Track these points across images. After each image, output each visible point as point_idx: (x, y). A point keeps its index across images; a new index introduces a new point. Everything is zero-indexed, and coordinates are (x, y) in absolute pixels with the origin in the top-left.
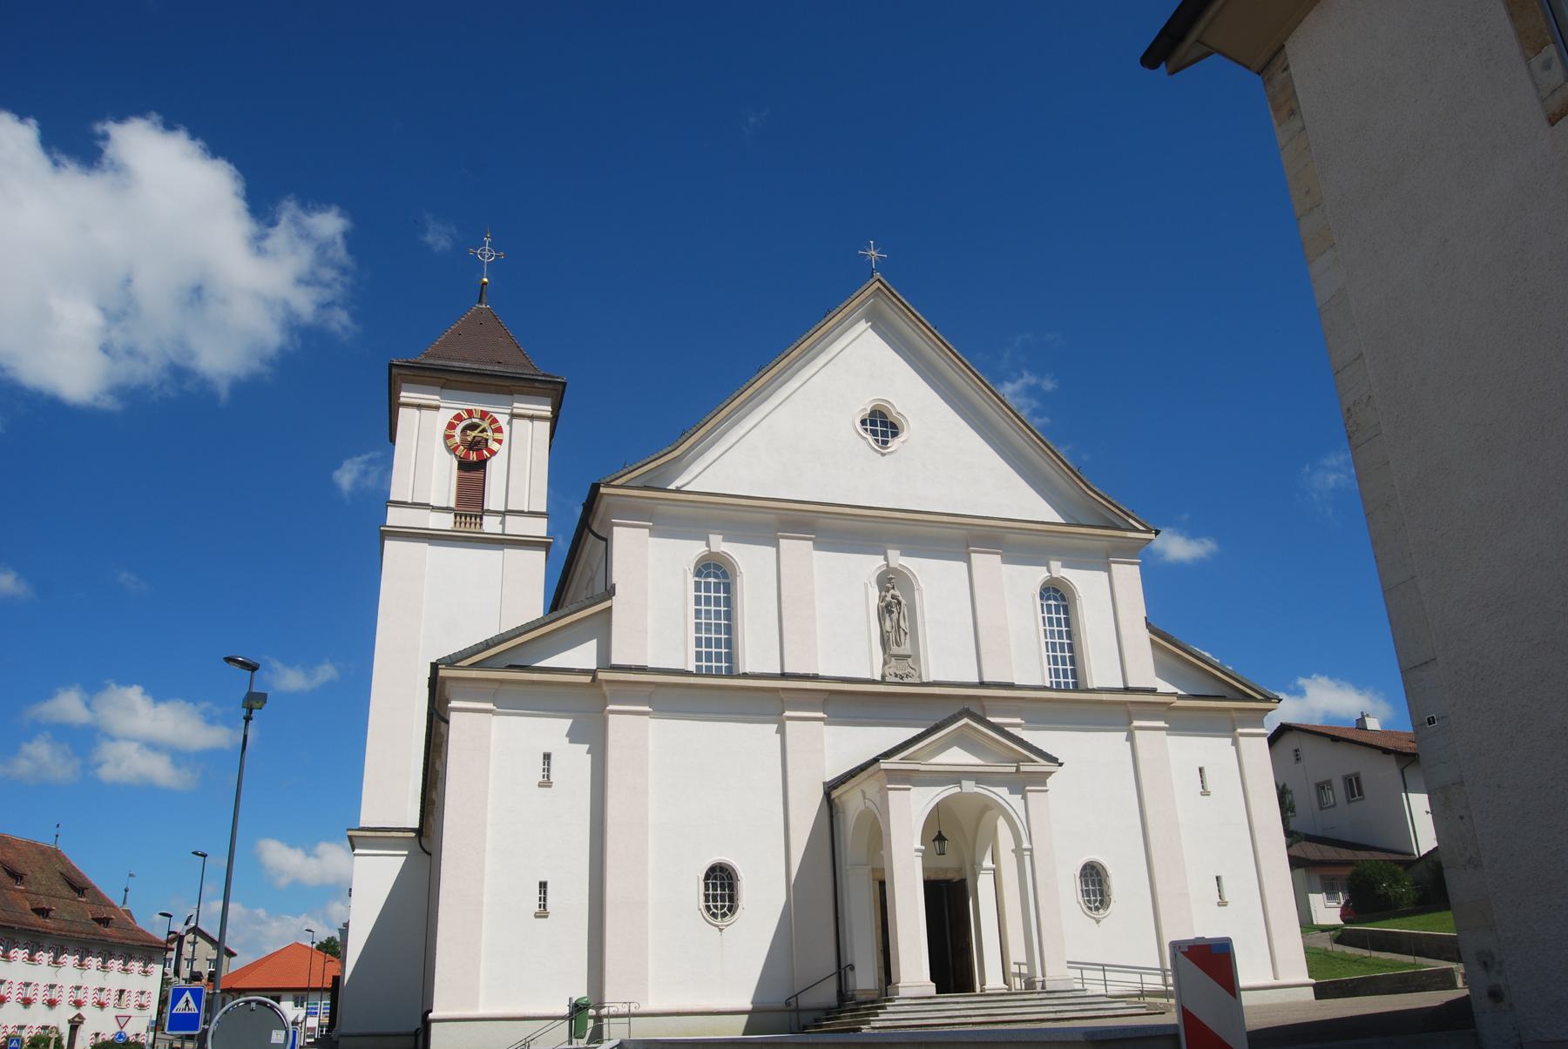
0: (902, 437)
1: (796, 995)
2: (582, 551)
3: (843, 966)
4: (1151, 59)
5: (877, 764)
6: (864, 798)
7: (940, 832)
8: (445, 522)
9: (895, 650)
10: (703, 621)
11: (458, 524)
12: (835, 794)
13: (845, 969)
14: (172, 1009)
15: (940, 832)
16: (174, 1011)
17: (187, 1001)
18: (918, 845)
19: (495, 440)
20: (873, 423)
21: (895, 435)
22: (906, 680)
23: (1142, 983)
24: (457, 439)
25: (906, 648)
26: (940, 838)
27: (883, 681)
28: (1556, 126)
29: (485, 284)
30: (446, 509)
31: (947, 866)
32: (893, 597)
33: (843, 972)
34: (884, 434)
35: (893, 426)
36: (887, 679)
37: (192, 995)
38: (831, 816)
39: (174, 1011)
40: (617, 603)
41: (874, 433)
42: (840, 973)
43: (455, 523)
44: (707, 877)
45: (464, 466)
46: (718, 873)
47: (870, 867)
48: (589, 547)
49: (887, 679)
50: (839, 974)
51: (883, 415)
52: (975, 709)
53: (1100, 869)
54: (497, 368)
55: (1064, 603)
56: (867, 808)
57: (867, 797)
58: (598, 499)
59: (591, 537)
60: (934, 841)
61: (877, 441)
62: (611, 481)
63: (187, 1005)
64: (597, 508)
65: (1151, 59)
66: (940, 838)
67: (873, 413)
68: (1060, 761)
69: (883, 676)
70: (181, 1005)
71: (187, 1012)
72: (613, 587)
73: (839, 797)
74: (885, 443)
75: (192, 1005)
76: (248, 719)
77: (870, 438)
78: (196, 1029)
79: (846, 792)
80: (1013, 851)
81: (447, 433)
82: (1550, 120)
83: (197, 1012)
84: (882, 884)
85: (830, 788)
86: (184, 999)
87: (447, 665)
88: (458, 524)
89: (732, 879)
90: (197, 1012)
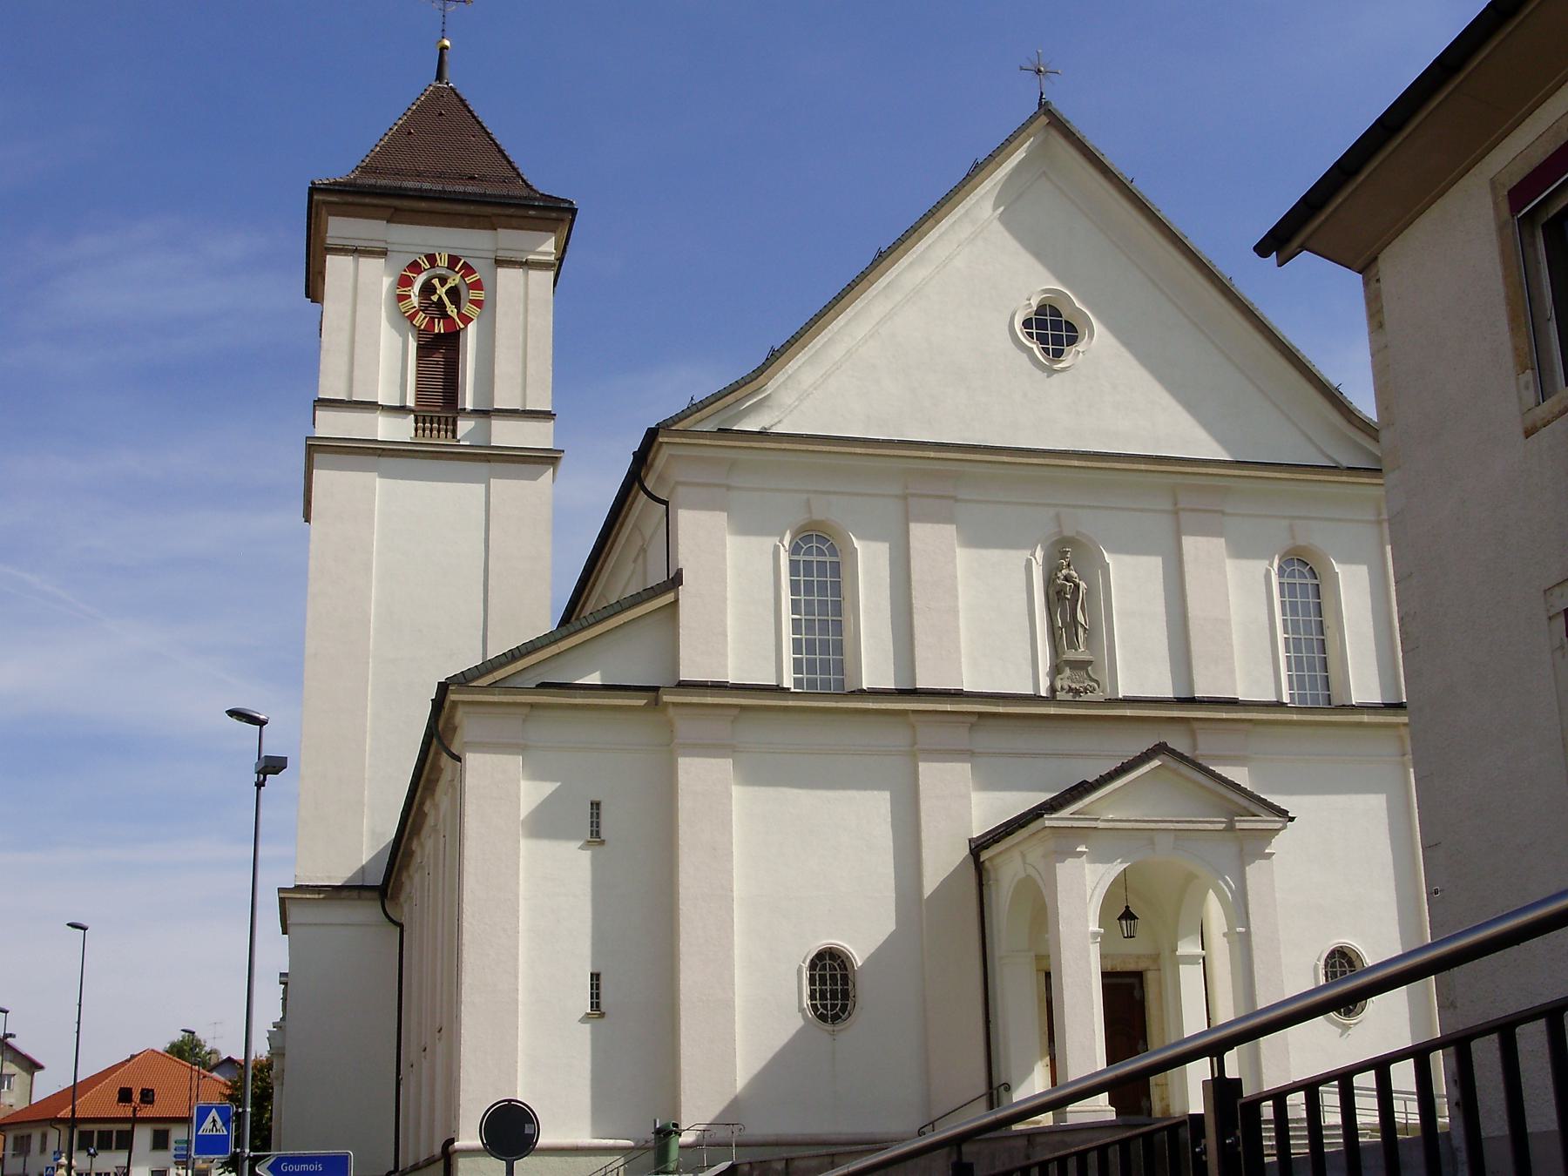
0: (1080, 346)
1: (932, 1123)
2: (626, 516)
3: (995, 1085)
4: (1262, 249)
5: (1040, 820)
6: (1024, 863)
7: (1127, 907)
8: (400, 430)
9: (1070, 655)
10: (802, 597)
11: (420, 432)
12: (985, 856)
13: (998, 1089)
14: (197, 1131)
15: (1127, 907)
16: (200, 1133)
17: (214, 1121)
18: (1094, 927)
19: (473, 302)
20: (1041, 324)
21: (1072, 341)
22: (1084, 697)
23: (1406, 1113)
24: (415, 301)
25: (1081, 653)
26: (1128, 915)
27: (1052, 698)
28: (1529, 439)
29: (446, 48)
30: (402, 409)
31: (1131, 954)
32: (1067, 578)
33: (995, 1092)
34: (1057, 340)
35: (1071, 327)
36: (1060, 696)
37: (218, 1112)
38: (980, 885)
39: (200, 1133)
40: (685, 592)
41: (1042, 339)
42: (991, 1095)
43: (416, 430)
44: (813, 966)
45: (426, 348)
46: (828, 962)
47: (1032, 954)
48: (640, 507)
49: (1060, 696)
50: (991, 1095)
51: (1056, 312)
52: (1179, 743)
53: (1354, 957)
54: (469, 189)
55: (1315, 582)
56: (1028, 876)
57: (1028, 862)
58: (654, 449)
59: (643, 497)
60: (1118, 919)
61: (1046, 351)
62: (672, 425)
63: (214, 1125)
64: (654, 459)
65: (1262, 249)
66: (1128, 915)
67: (1041, 309)
68: (1290, 815)
69: (1053, 689)
70: (208, 1124)
71: (214, 1133)
72: (679, 573)
73: (990, 859)
74: (1058, 354)
75: (219, 1123)
76: (259, 785)
77: (1035, 347)
78: (197, 1152)
79: (1001, 853)
80: (1224, 935)
81: (398, 292)
82: (1526, 432)
83: (226, 1133)
84: (1048, 975)
85: (978, 847)
86: (210, 1119)
87: (460, 684)
88: (420, 432)
89: (846, 970)
90: (226, 1133)
